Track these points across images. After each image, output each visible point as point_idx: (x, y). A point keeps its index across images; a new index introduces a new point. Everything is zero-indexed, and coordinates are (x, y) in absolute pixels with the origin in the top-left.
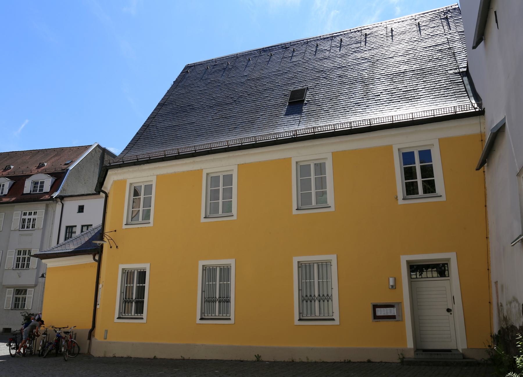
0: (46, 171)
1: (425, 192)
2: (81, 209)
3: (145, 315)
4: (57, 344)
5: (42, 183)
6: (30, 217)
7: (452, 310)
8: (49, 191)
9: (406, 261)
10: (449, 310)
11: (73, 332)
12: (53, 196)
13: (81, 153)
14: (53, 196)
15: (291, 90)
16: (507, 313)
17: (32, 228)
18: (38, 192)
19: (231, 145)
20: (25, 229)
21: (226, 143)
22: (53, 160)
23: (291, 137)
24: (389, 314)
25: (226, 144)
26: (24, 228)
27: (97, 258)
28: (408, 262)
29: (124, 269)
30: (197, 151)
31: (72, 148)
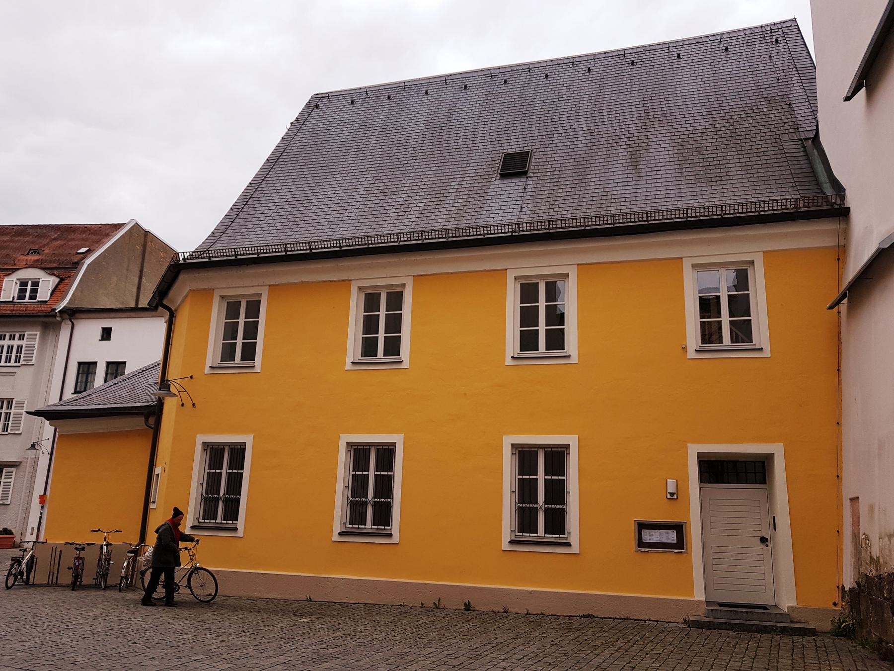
0: (41, 264)
1: (735, 339)
2: (106, 334)
3: (241, 523)
4: (104, 566)
5: (36, 284)
6: (11, 343)
7: (769, 539)
8: (47, 300)
9: (774, 454)
10: (763, 540)
11: (56, 548)
12: (55, 309)
13: (106, 236)
14: (55, 309)
15: (503, 153)
16: (881, 550)
17: (15, 362)
18: (27, 299)
19: (404, 241)
20: (12, 363)
21: (395, 237)
22: (54, 245)
23: (510, 234)
24: (665, 541)
25: (396, 240)
26: (9, 362)
27: (152, 421)
28: (700, 455)
29: (206, 443)
30: (343, 249)
31: (90, 226)
